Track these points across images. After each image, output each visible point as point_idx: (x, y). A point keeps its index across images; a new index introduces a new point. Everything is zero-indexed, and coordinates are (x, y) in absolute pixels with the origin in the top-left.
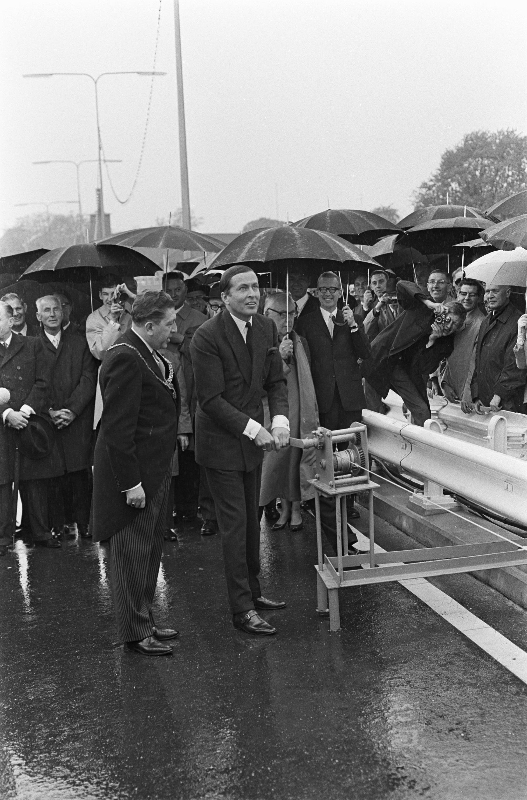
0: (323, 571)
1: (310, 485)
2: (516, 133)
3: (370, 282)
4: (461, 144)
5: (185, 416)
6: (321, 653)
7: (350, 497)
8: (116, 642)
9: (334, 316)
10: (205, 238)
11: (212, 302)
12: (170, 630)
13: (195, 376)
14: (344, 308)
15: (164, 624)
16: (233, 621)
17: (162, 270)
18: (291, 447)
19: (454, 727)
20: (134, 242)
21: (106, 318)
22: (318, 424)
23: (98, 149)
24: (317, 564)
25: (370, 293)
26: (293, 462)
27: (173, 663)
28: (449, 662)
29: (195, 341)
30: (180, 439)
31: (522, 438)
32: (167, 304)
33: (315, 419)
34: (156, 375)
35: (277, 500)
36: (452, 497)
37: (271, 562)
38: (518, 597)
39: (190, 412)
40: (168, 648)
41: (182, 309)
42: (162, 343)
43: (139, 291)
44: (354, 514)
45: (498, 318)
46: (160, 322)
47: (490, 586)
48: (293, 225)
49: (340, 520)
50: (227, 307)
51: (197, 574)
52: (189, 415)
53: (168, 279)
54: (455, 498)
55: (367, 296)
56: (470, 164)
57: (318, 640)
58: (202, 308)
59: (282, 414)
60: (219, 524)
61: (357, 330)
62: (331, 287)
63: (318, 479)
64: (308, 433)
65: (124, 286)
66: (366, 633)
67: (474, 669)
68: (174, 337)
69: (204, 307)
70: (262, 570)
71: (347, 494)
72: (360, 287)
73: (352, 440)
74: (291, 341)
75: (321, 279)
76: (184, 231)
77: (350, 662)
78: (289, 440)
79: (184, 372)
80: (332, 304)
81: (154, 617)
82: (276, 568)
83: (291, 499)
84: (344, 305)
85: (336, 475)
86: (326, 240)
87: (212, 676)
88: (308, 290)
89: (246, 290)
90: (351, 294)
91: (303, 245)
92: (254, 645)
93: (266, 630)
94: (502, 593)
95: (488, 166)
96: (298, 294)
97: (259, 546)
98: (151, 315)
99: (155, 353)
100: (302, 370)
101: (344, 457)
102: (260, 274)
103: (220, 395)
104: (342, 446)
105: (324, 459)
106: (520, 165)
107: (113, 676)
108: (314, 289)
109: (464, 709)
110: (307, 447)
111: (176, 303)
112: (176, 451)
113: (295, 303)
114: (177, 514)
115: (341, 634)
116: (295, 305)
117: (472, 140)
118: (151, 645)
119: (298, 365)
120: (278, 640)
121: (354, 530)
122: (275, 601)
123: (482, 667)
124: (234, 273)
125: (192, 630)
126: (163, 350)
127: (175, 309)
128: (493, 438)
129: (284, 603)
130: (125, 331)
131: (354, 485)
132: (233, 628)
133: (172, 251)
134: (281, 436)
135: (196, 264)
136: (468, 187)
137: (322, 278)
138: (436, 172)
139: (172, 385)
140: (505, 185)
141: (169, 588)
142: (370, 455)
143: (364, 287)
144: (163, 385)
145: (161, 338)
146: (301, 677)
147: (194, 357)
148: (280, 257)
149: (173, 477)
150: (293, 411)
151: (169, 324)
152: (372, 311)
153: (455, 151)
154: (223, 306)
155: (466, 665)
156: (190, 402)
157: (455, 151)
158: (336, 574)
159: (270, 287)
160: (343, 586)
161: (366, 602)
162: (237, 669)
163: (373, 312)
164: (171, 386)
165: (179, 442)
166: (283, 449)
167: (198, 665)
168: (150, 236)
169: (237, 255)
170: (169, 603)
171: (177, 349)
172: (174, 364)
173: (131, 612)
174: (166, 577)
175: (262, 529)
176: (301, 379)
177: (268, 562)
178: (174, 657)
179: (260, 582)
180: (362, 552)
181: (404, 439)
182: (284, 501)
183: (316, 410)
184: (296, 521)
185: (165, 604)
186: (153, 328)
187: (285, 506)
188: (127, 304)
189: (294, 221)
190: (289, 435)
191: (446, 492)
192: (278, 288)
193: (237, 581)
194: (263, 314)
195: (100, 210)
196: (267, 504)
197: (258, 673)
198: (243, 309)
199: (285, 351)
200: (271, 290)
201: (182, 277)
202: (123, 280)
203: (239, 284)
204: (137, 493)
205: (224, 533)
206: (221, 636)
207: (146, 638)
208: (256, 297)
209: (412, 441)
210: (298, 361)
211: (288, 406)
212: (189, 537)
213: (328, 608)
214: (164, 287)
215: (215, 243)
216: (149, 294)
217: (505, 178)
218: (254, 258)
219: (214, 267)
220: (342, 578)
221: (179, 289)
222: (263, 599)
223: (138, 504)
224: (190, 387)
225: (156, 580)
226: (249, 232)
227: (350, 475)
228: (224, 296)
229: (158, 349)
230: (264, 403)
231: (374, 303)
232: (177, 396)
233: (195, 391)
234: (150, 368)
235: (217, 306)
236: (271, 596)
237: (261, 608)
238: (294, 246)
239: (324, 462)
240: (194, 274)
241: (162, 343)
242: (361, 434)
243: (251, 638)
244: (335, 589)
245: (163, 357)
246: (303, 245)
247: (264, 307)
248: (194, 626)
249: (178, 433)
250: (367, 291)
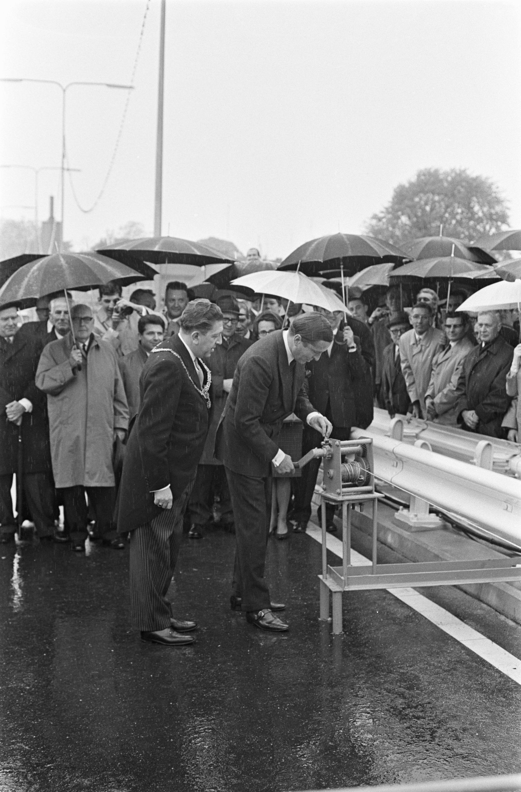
2: (468, 172)
4: (414, 179)
12: (189, 623)
19: (468, 726)
21: (105, 324)
23: (61, 157)
28: (452, 668)
31: (506, 464)
32: (217, 317)
34: (195, 384)
36: (437, 515)
38: (511, 613)
45: (489, 349)
46: (206, 333)
47: (481, 601)
54: (440, 517)
56: (421, 199)
61: (354, 350)
67: (478, 675)
94: (493, 608)
95: (439, 202)
98: (199, 325)
106: (469, 203)
109: (474, 711)
117: (424, 175)
123: (485, 675)
128: (479, 462)
136: (417, 222)
138: (388, 204)
139: (208, 394)
140: (454, 222)
144: (200, 394)
145: (205, 348)
151: (215, 336)
153: (407, 185)
155: (469, 672)
157: (407, 185)
160: (347, 590)
167: (210, 659)
181: (397, 457)
186: (199, 337)
191: (432, 511)
195: (52, 218)
209: (404, 460)
217: (453, 215)
223: (164, 505)
234: (190, 378)
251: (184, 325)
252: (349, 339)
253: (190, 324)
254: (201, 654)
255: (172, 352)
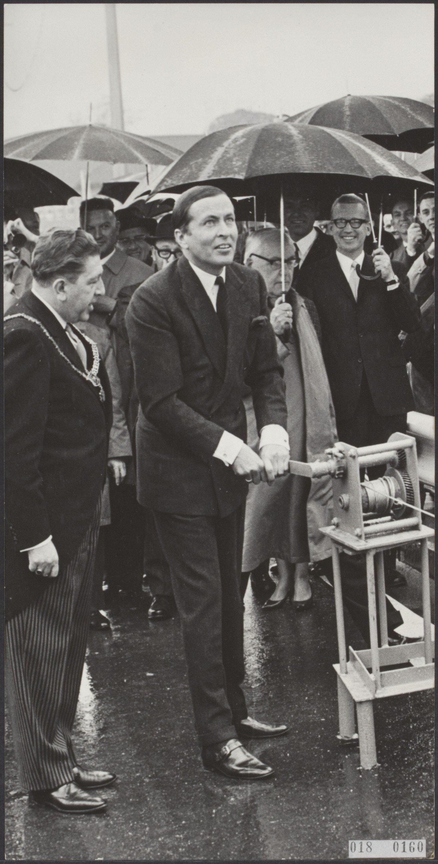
0: (347, 673)
1: (323, 536)
3: (418, 211)
5: (117, 428)
6: (347, 805)
7: (388, 555)
8: (15, 790)
9: (358, 266)
10: (147, 143)
11: (160, 245)
13: (134, 365)
14: (375, 252)
15: (92, 763)
16: (203, 757)
17: (77, 195)
18: (292, 476)
20: (34, 153)
22: (335, 437)
24: (338, 662)
25: (419, 229)
26: (294, 500)
27: (106, 826)
29: (134, 309)
30: (112, 467)
32: (88, 249)
33: (329, 429)
34: (73, 363)
35: (271, 562)
37: (262, 661)
39: (127, 423)
40: (98, 801)
41: (111, 258)
42: (81, 312)
43: (43, 229)
44: (397, 580)
48: (291, 119)
49: (374, 590)
50: (186, 253)
51: (143, 683)
52: (126, 427)
53: (88, 209)
55: (413, 233)
57: (341, 785)
58: (144, 255)
59: (276, 423)
60: (177, 602)
61: (396, 286)
62: (354, 219)
63: (337, 526)
64: (318, 453)
65: (18, 224)
66: (420, 769)
68: (101, 302)
69: (147, 253)
70: (248, 676)
71: (385, 549)
72: (402, 218)
73: (392, 462)
74: (288, 306)
75: (337, 206)
76: (114, 133)
77: (395, 817)
78: (289, 464)
79: (117, 357)
80: (355, 245)
81: (75, 752)
82: (271, 671)
83: (294, 559)
84: (375, 246)
85: (365, 518)
86: (343, 144)
87: (170, 846)
88: (316, 224)
89: (215, 225)
90: (387, 230)
91: (306, 152)
92: (238, 795)
93: (256, 771)
96: (300, 230)
97: (242, 636)
98: (63, 267)
99: (70, 329)
100: (308, 352)
101: (380, 489)
102: (238, 199)
103: (175, 395)
104: (375, 471)
105: (346, 493)
107: (11, 844)
108: (325, 222)
110: (318, 476)
111: (103, 248)
112: (106, 486)
113: (295, 245)
114: (109, 587)
115: (379, 773)
116: (294, 248)
118: (72, 797)
119: (301, 344)
120: (275, 787)
121: (397, 605)
122: (270, 724)
124: (194, 198)
125: (137, 772)
126: (83, 323)
127: (102, 257)
129: (284, 727)
130: (21, 295)
131: (396, 533)
132: (202, 769)
133: (94, 164)
134: (275, 459)
135: (133, 185)
137: (338, 205)
139: (98, 379)
141: (99, 705)
142: (422, 484)
143: (408, 217)
144: (84, 379)
145: (79, 305)
146: (315, 845)
147: (132, 334)
148: (270, 172)
149: (102, 527)
150: (294, 419)
151: (92, 282)
152: (421, 257)
154: (178, 251)
156: (128, 407)
158: (368, 678)
159: (253, 220)
161: (419, 718)
162: (210, 834)
163: (425, 258)
164: (96, 381)
165: (111, 471)
166: (278, 479)
167: (147, 829)
168: (60, 144)
169: (200, 169)
170: (100, 729)
171: (104, 322)
172: (101, 345)
173: (39, 743)
174: (95, 687)
175: (246, 609)
176: (307, 367)
177: (258, 662)
178: (108, 816)
179: (246, 694)
180: (410, 640)
182: (282, 562)
183: (332, 416)
184: (302, 594)
185: (92, 731)
186: (66, 288)
187: (283, 571)
188: (24, 251)
189: (292, 114)
190: (289, 457)
192: (267, 221)
193: (208, 692)
194: (243, 264)
196: (253, 569)
197: (245, 841)
198: (210, 255)
199: (279, 322)
200: (256, 224)
201: (111, 206)
202: (17, 212)
203: (204, 215)
204: (44, 554)
205: (185, 616)
206: (183, 781)
207: (63, 785)
208: (231, 237)
210: (301, 338)
211: (285, 410)
212: (129, 623)
213: (356, 731)
214: (82, 222)
215: (163, 151)
216: (58, 234)
218: (228, 173)
219: (163, 188)
220: (379, 683)
221: (106, 225)
222: (252, 722)
223: (47, 571)
224: (126, 383)
225: (75, 700)
226: (219, 132)
227: (389, 518)
228: (179, 235)
229: (74, 322)
230: (246, 406)
231: (426, 244)
232: (106, 397)
233: (136, 389)
235: (168, 251)
236: (263, 715)
237: (248, 737)
238: (292, 153)
239: (345, 498)
240: (130, 200)
241: (81, 312)
242: (407, 451)
243: (233, 784)
244: (367, 701)
245: (83, 335)
246: (306, 152)
247: (244, 252)
248: (141, 765)
249: (110, 456)
250: (413, 225)
251: (38, 272)
252: (384, 272)
253: (48, 270)
254: (133, 822)
255: (26, 317)
